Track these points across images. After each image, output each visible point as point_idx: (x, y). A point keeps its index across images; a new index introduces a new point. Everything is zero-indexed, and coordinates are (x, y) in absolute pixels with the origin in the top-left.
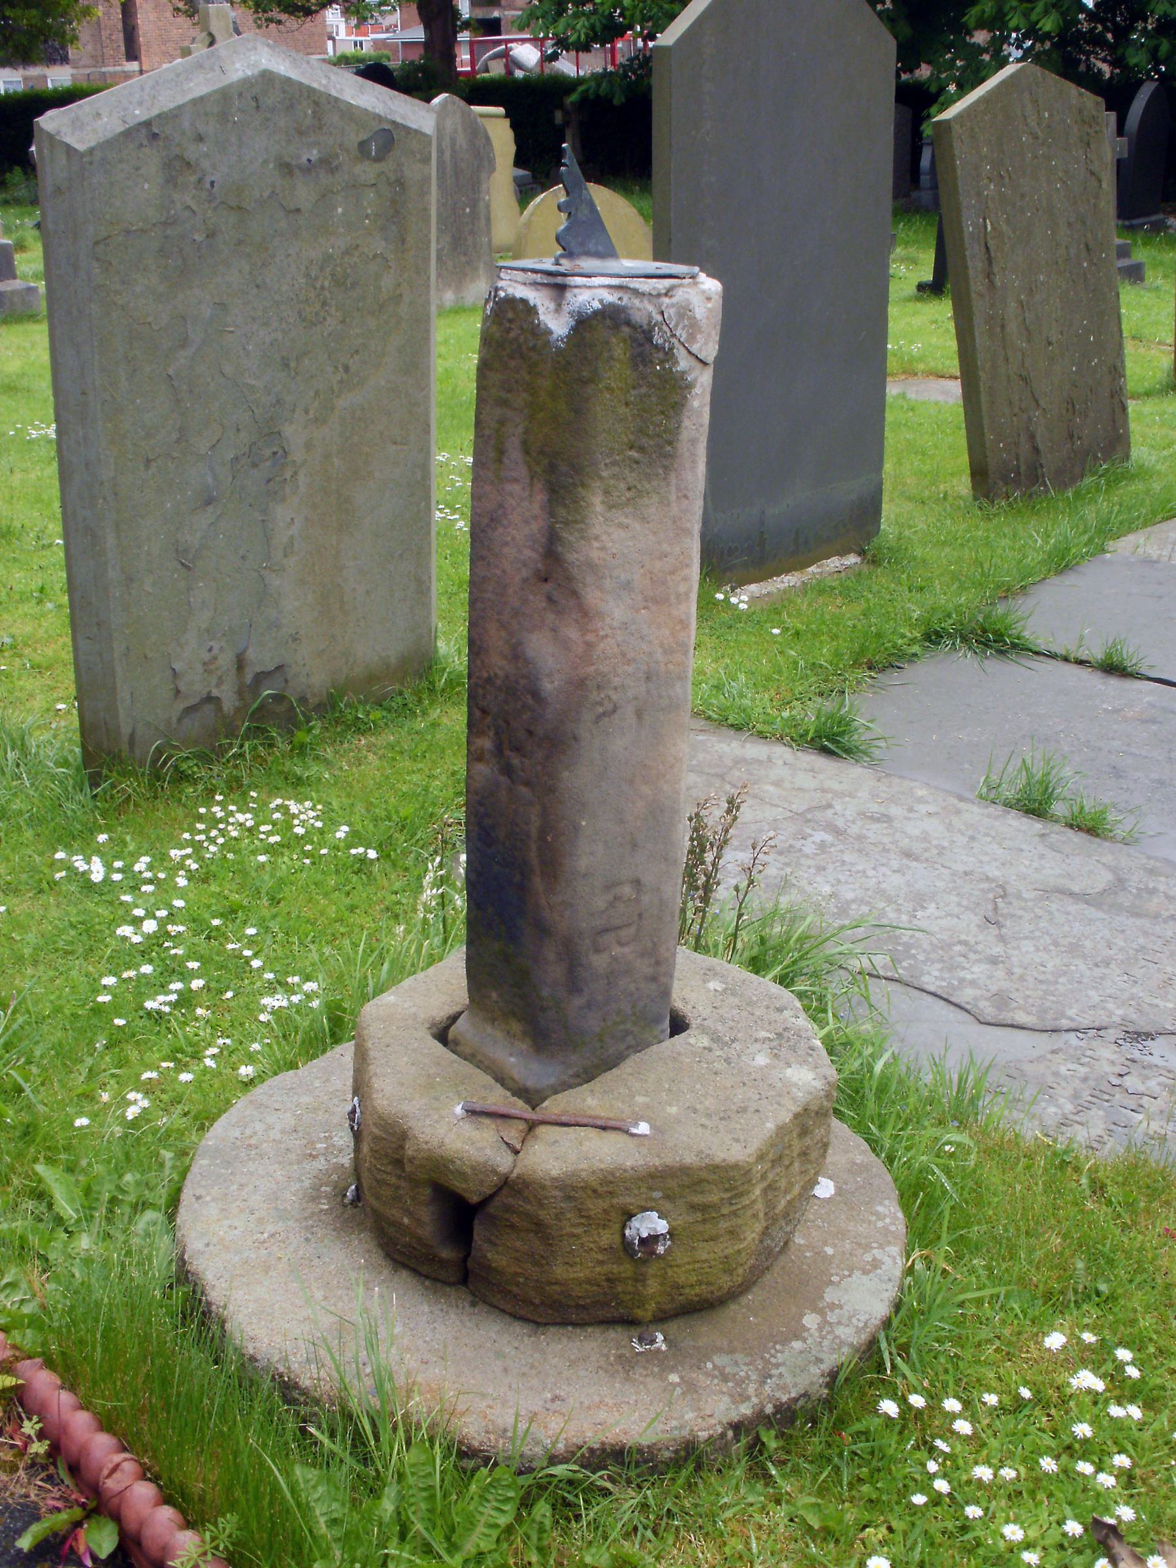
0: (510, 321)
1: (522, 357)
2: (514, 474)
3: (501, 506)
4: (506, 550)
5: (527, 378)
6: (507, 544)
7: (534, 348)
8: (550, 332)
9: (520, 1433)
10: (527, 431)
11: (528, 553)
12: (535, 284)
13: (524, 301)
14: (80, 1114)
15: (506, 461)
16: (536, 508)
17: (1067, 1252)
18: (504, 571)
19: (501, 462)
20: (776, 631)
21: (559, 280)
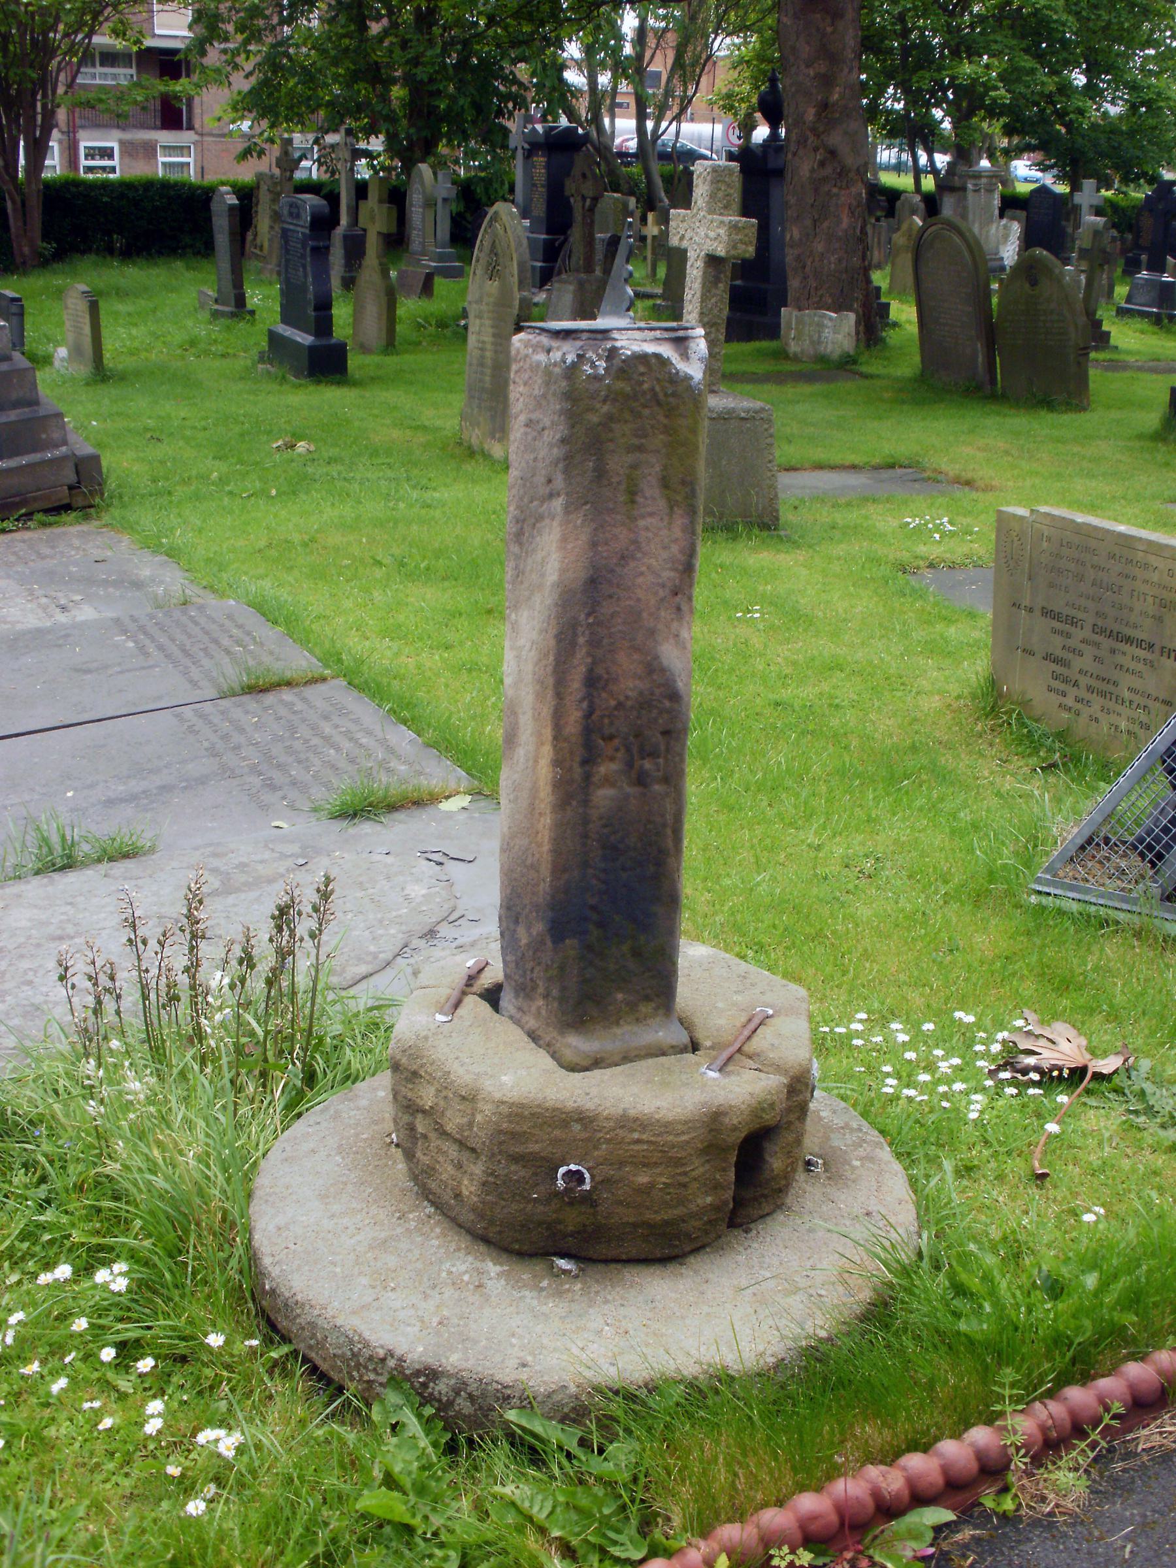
0: (642, 374)
1: (659, 404)
2: (649, 510)
3: (634, 541)
4: (640, 580)
5: (665, 421)
6: (642, 574)
7: (674, 394)
8: (691, 378)
9: (905, 1236)
10: (665, 468)
11: (667, 574)
12: (657, 340)
13: (657, 356)
14: (885, 1063)
15: (640, 499)
16: (677, 532)
17: (76, 1342)
18: (639, 600)
19: (633, 502)
20: (70, 794)
21: (681, 333)
